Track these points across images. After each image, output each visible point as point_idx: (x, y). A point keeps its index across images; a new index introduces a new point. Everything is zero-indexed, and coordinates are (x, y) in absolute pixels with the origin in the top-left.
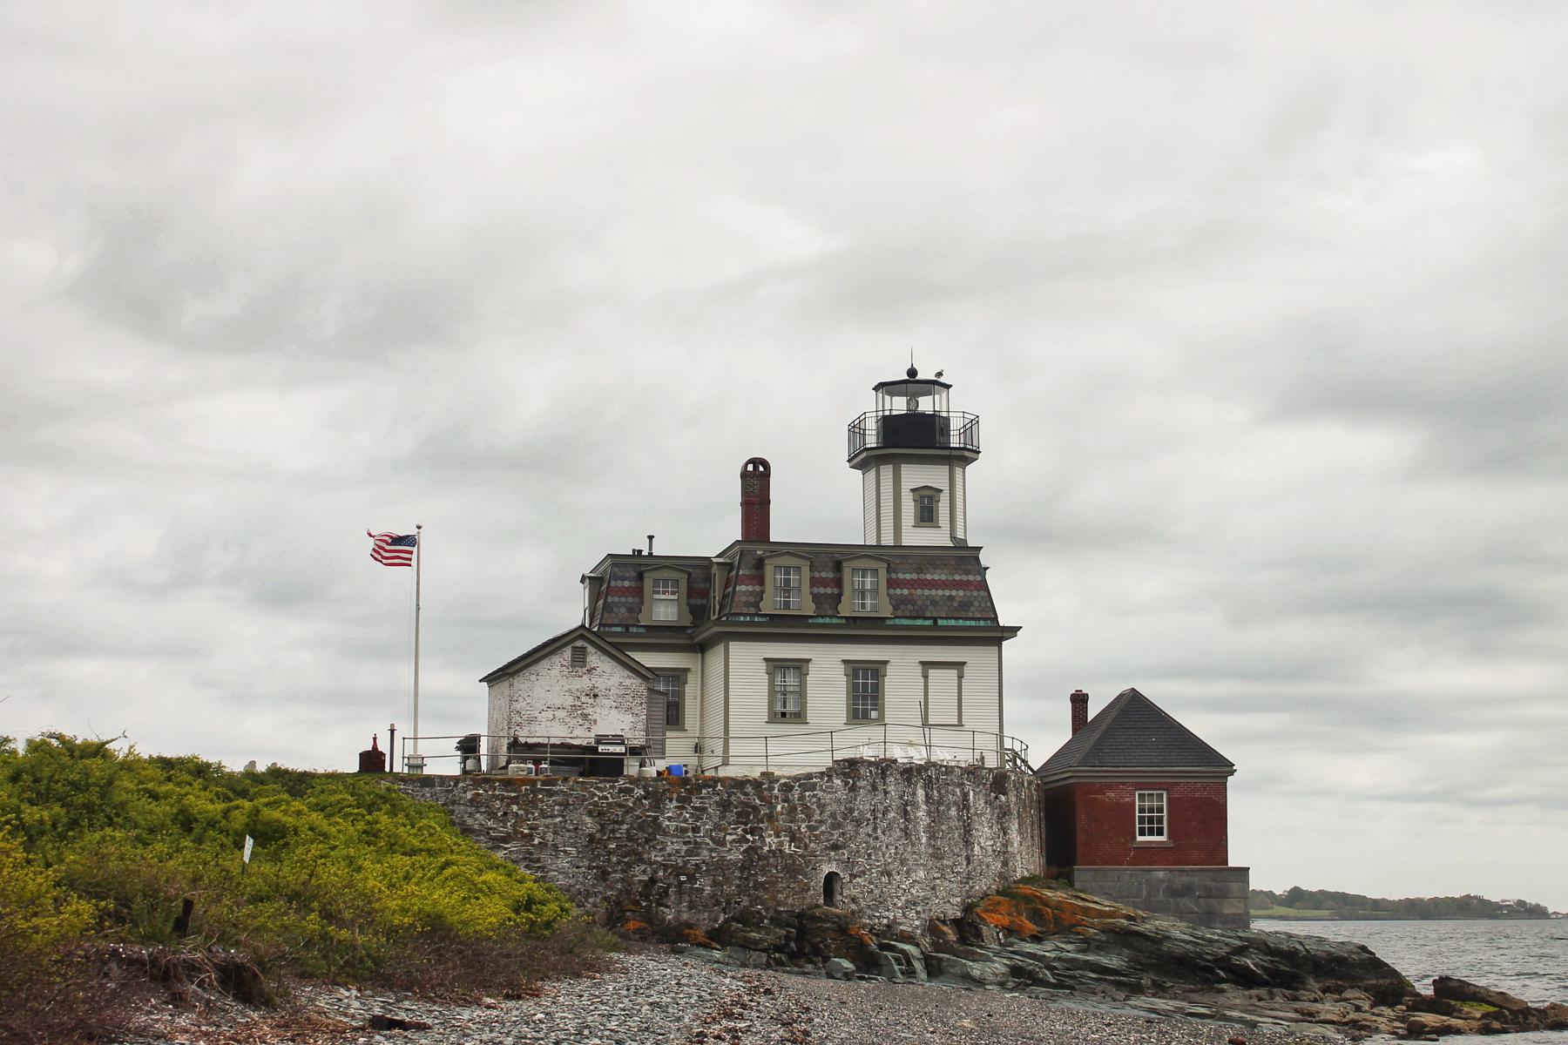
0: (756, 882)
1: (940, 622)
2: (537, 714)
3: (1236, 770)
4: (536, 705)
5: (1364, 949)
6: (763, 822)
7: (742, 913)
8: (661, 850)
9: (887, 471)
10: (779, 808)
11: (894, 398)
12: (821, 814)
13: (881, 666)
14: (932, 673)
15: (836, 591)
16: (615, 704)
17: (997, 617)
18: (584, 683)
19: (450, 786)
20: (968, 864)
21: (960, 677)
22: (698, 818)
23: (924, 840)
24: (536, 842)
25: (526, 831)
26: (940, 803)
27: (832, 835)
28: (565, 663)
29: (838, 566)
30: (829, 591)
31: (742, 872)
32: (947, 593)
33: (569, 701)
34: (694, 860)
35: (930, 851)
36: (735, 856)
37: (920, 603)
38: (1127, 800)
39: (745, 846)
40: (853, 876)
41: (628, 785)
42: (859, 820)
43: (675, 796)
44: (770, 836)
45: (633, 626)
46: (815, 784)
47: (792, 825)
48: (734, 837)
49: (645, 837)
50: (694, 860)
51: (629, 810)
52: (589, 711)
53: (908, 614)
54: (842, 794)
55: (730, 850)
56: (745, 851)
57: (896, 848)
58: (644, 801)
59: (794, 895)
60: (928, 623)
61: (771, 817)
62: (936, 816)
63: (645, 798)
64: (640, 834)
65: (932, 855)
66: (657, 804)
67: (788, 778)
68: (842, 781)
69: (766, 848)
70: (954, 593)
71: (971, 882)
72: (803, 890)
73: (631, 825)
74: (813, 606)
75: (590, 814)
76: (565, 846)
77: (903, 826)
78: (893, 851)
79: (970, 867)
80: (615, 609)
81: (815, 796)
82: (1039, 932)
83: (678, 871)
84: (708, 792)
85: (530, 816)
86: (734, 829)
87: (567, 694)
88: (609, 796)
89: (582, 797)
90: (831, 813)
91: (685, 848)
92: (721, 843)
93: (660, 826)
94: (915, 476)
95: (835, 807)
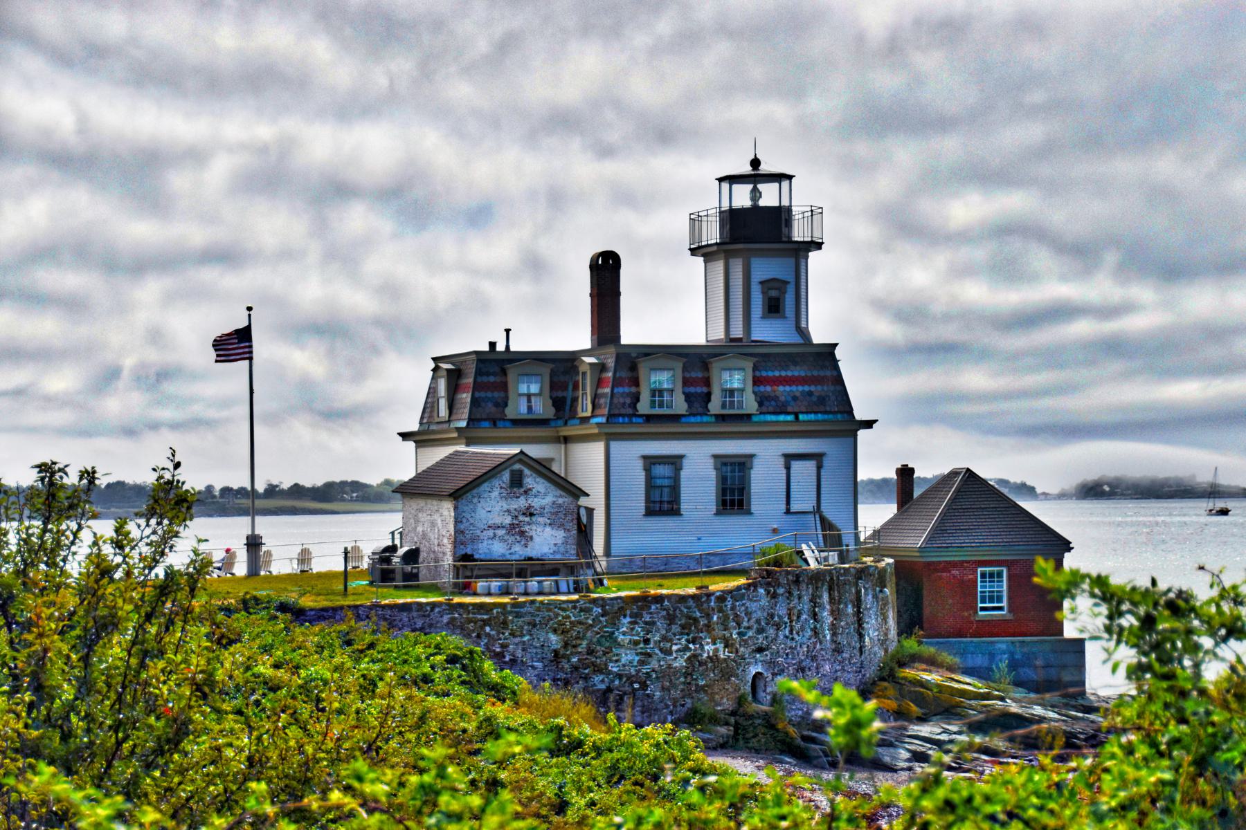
0: (697, 685)
1: (801, 417)
2: (478, 532)
3: (1073, 548)
4: (478, 525)
6: (702, 632)
7: (687, 714)
8: (617, 661)
10: (715, 618)
11: (777, 204)
12: (749, 620)
13: (747, 459)
15: (705, 390)
16: (549, 521)
17: (852, 410)
18: (522, 503)
19: (427, 611)
20: (861, 654)
22: (648, 632)
23: (828, 637)
24: (507, 659)
25: (498, 650)
26: (839, 603)
27: (758, 639)
28: (504, 486)
30: (699, 390)
31: (686, 677)
32: (807, 388)
33: (508, 520)
34: (645, 669)
35: (833, 647)
36: (680, 663)
37: (783, 399)
38: (971, 577)
39: (688, 654)
40: (774, 675)
41: (588, 605)
42: (779, 624)
43: (628, 612)
44: (708, 644)
45: (500, 419)
46: (744, 594)
47: (726, 632)
48: (679, 646)
49: (603, 651)
50: (645, 669)
52: (526, 528)
53: (771, 409)
54: (764, 602)
55: (676, 658)
56: (689, 658)
57: (808, 646)
58: (601, 619)
59: (728, 695)
60: (790, 418)
61: (708, 627)
62: (837, 614)
63: (602, 616)
64: (598, 648)
65: (834, 650)
66: (614, 623)
67: (722, 591)
68: (765, 590)
69: (705, 655)
70: (813, 388)
71: (863, 670)
72: (735, 690)
73: (591, 641)
74: (685, 406)
75: (555, 631)
76: (533, 661)
77: (812, 626)
78: (805, 649)
79: (863, 657)
80: (483, 404)
81: (743, 605)
82: (923, 714)
83: (631, 679)
84: (657, 608)
85: (501, 635)
86: (679, 639)
87: (506, 514)
88: (571, 615)
89: (547, 618)
90: (757, 620)
91: (637, 658)
92: (669, 652)
93: (615, 640)
94: (765, 269)
95: (759, 613)
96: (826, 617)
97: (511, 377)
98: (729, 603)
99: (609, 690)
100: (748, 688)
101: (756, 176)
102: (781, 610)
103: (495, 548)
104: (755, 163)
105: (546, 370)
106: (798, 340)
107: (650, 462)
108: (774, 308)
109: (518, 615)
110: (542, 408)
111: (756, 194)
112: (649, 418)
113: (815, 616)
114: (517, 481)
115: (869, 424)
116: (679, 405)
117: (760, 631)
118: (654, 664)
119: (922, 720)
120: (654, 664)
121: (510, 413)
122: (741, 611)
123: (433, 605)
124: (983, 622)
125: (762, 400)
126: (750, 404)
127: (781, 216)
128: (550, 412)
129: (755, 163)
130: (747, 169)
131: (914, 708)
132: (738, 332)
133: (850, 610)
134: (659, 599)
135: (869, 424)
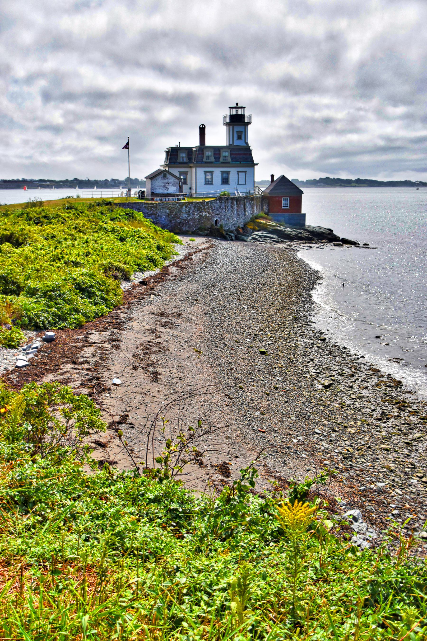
5: (331, 230)
9: (231, 127)
14: (240, 173)
18: (166, 181)
21: (246, 174)
29: (220, 151)
33: (163, 185)
34: (189, 218)
36: (197, 217)
51: (175, 209)
54: (219, 204)
61: (204, 209)
66: (181, 208)
83: (185, 220)
96: (235, 207)
97: (221, 152)
98: (209, 204)
99: (180, 222)
100: (214, 223)
101: (237, 107)
102: (223, 206)
103: (160, 191)
104: (237, 104)
105: (187, 151)
106: (245, 145)
107: (222, 172)
108: (239, 138)
109: (160, 206)
110: (185, 160)
111: (237, 111)
112: (206, 162)
113: (232, 207)
114: (165, 176)
115: (257, 164)
116: (212, 159)
117: (218, 210)
118: (191, 217)
119: (258, 231)
120: (191, 217)
121: (178, 161)
122: (212, 206)
123: (141, 203)
124: (283, 210)
125: (232, 159)
126: (229, 160)
127: (243, 116)
128: (188, 161)
129: (237, 104)
130: (235, 105)
131: (257, 228)
132: (231, 143)
133: (242, 206)
134: (192, 203)
135: (257, 164)
